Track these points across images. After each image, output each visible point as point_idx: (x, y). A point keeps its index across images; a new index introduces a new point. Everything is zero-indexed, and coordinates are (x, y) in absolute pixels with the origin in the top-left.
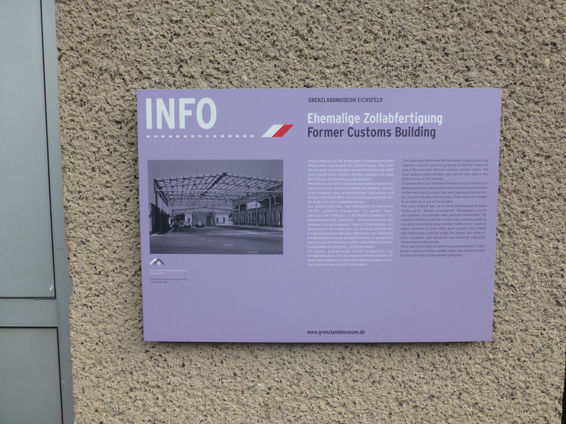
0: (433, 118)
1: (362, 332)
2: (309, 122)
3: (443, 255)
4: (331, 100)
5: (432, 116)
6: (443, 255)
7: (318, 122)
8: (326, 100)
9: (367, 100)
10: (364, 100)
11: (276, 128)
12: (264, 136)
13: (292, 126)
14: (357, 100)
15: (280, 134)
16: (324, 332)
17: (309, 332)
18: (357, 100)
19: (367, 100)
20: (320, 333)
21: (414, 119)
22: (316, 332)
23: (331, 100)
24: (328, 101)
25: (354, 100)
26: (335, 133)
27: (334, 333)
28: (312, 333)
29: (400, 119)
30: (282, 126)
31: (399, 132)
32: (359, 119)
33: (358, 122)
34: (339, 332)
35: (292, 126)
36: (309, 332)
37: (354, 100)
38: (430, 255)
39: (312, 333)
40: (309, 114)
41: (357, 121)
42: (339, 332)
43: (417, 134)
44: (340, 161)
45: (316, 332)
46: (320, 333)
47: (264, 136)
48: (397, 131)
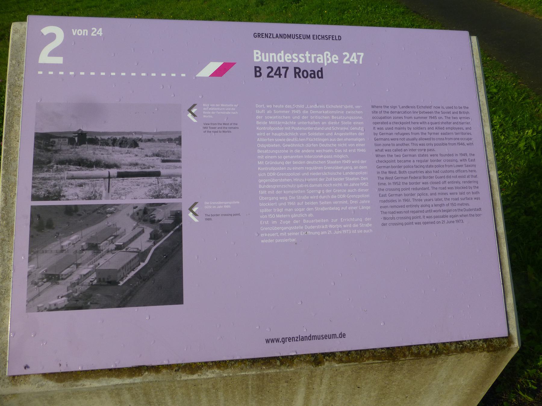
0: (273, 56)
1: (342, 335)
2: (255, 60)
3: (432, 223)
4: (281, 36)
5: (271, 55)
6: (432, 223)
7: (275, 61)
8: (275, 36)
9: (323, 37)
10: (320, 37)
11: (214, 66)
12: (199, 75)
13: (233, 64)
14: (311, 37)
15: (219, 73)
16: (289, 339)
17: (267, 341)
18: (311, 37)
19: (323, 37)
20: (284, 340)
21: (310, 58)
22: (278, 340)
23: (281, 36)
24: (277, 36)
25: (308, 37)
26: (314, 74)
27: (303, 339)
28: (273, 341)
29: (286, 58)
30: (221, 63)
31: (298, 72)
32: (337, 59)
33: (337, 62)
34: (311, 338)
35: (233, 64)
36: (267, 341)
37: (308, 37)
38: (390, 224)
39: (273, 341)
40: (255, 51)
41: (335, 60)
42: (311, 338)
43: (320, 76)
44: (217, 105)
45: (278, 340)
46: (284, 340)
47: (199, 75)
48: (256, 71)
